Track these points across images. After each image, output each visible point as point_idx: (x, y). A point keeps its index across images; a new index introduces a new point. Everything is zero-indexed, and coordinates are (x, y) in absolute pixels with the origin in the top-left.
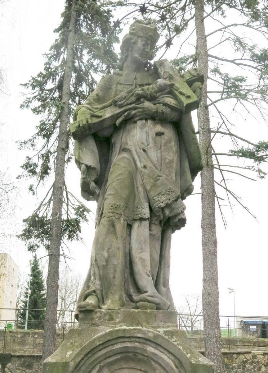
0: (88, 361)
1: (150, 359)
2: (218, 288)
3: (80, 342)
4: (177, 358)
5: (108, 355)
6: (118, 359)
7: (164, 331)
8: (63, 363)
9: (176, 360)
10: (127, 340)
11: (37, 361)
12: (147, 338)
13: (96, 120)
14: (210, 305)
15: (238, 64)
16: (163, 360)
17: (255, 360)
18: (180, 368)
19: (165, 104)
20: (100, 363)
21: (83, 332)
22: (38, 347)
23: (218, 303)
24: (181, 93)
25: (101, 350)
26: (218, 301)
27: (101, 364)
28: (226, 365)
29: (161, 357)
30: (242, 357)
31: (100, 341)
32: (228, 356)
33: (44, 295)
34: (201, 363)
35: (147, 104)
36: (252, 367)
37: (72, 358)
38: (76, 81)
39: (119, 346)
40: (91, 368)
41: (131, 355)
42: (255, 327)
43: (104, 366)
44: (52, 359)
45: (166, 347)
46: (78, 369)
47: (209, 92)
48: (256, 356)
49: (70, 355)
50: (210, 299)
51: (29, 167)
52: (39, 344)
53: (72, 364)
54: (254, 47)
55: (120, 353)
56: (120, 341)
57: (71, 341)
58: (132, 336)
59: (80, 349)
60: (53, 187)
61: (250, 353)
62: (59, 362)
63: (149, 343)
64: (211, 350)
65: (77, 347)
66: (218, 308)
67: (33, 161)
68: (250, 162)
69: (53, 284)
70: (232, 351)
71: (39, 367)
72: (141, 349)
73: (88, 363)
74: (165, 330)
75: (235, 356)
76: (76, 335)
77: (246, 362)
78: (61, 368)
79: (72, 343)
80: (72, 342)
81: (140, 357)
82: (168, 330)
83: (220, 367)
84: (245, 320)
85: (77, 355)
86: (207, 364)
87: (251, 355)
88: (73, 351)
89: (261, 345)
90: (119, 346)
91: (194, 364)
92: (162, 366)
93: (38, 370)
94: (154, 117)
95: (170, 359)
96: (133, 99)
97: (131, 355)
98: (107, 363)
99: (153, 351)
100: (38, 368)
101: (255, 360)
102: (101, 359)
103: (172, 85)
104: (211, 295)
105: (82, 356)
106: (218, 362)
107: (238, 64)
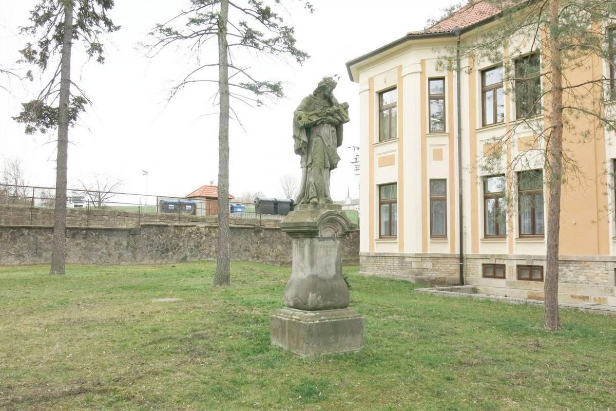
13: (310, 122)
15: (247, 13)
17: (199, 231)
19: (337, 119)
24: (343, 115)
30: (189, 229)
32: (179, 228)
35: (330, 118)
36: (196, 236)
42: (190, 207)
47: (228, 34)
48: (199, 228)
51: (29, 54)
54: (260, 3)
60: (60, 76)
61: (196, 226)
67: (33, 48)
68: (251, 94)
70: (181, 224)
75: (183, 228)
77: (192, 233)
84: (166, 200)
87: (196, 227)
89: (194, 220)
94: (331, 123)
96: (325, 114)
101: (199, 231)
103: (339, 110)
107: (247, 13)
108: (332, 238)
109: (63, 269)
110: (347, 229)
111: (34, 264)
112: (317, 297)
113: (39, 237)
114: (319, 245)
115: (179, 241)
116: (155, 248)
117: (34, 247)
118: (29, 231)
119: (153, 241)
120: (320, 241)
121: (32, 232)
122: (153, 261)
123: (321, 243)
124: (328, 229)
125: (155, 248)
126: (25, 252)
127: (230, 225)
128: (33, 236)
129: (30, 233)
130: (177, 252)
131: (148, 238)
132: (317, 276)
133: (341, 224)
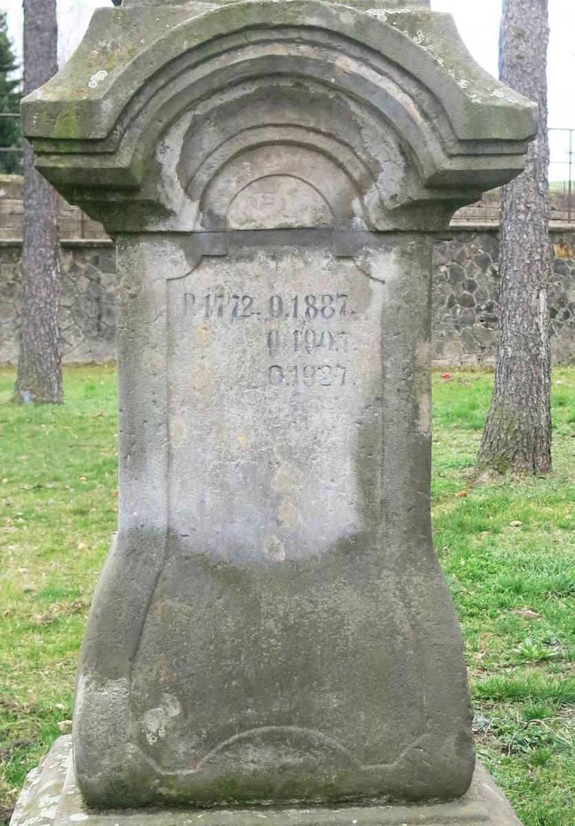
0: (156, 98)
1: (343, 97)
2: (546, 16)
3: (130, 46)
4: (427, 90)
5: (216, 83)
6: (248, 95)
7: (387, 14)
8: (80, 103)
9: (424, 96)
10: (276, 35)
11: (11, 259)
12: (335, 29)
14: (521, 65)
16: (386, 96)
18: (436, 117)
20: (193, 105)
21: (138, 20)
22: (11, 225)
23: (544, 60)
25: (195, 66)
26: (545, 53)
27: (197, 112)
28: (558, 263)
29: (377, 87)
31: (191, 37)
33: (15, 83)
34: (498, 103)
37: (107, 89)
38: (102, 221)
39: (251, 54)
40: (165, 120)
41: (286, 84)
43: (206, 117)
44: (48, 92)
45: (393, 57)
46: (126, 121)
49: (100, 82)
50: (523, 47)
52: (12, 214)
53: (108, 106)
55: (252, 79)
56: (252, 40)
57: (103, 44)
58: (288, 22)
59: (130, 62)
62: (70, 100)
63: (344, 45)
64: (519, 198)
65: (121, 59)
66: (544, 76)
69: (39, 22)
71: (17, 276)
72: (317, 63)
73: (157, 103)
74: (391, 12)
76: (117, 27)
78: (73, 117)
79: (104, 51)
80: (105, 48)
81: (315, 89)
82: (399, 12)
83: (542, 246)
85: (125, 79)
86: (517, 104)
88: (108, 71)
90: (251, 54)
91: (477, 105)
92: (381, 116)
93: (13, 285)
95: (404, 91)
97: (286, 84)
98: (213, 110)
99: (353, 70)
100: (13, 279)
102: (197, 93)
104: (526, 35)
105: (137, 84)
106: (537, 233)
108: (327, 235)
109: (51, 387)
110: (437, 155)
111: (93, 364)
112: (138, 707)
113: (103, 276)
114: (189, 298)
115: (567, 287)
116: (479, 310)
117: (91, 309)
118: (75, 258)
119: (472, 286)
120: (199, 260)
121: (84, 261)
122: (474, 358)
123: (208, 277)
124: (274, 162)
125: (479, 310)
126: (66, 324)
127: (552, 224)
128: (87, 274)
129: (79, 264)
130: (560, 326)
131: (455, 275)
132: (170, 533)
133: (381, 116)
